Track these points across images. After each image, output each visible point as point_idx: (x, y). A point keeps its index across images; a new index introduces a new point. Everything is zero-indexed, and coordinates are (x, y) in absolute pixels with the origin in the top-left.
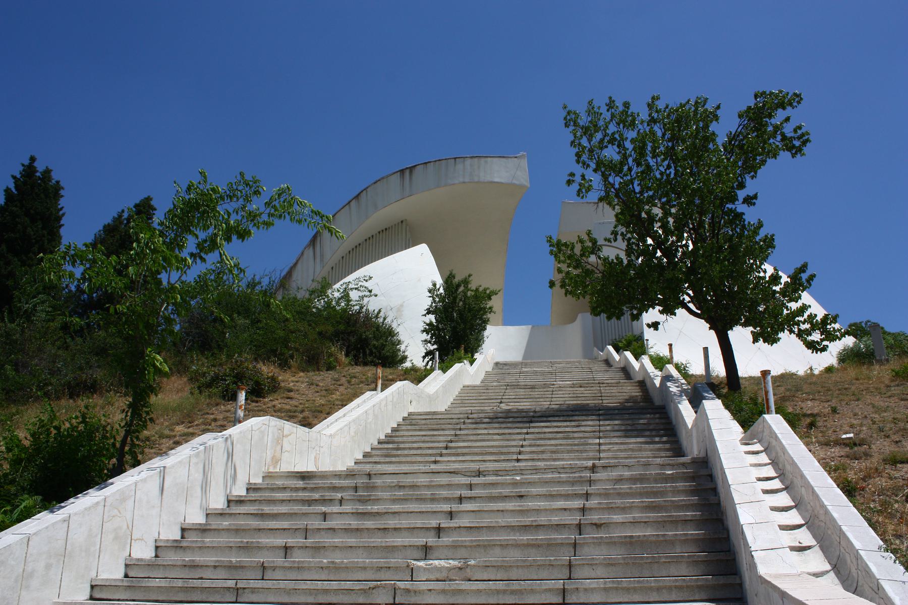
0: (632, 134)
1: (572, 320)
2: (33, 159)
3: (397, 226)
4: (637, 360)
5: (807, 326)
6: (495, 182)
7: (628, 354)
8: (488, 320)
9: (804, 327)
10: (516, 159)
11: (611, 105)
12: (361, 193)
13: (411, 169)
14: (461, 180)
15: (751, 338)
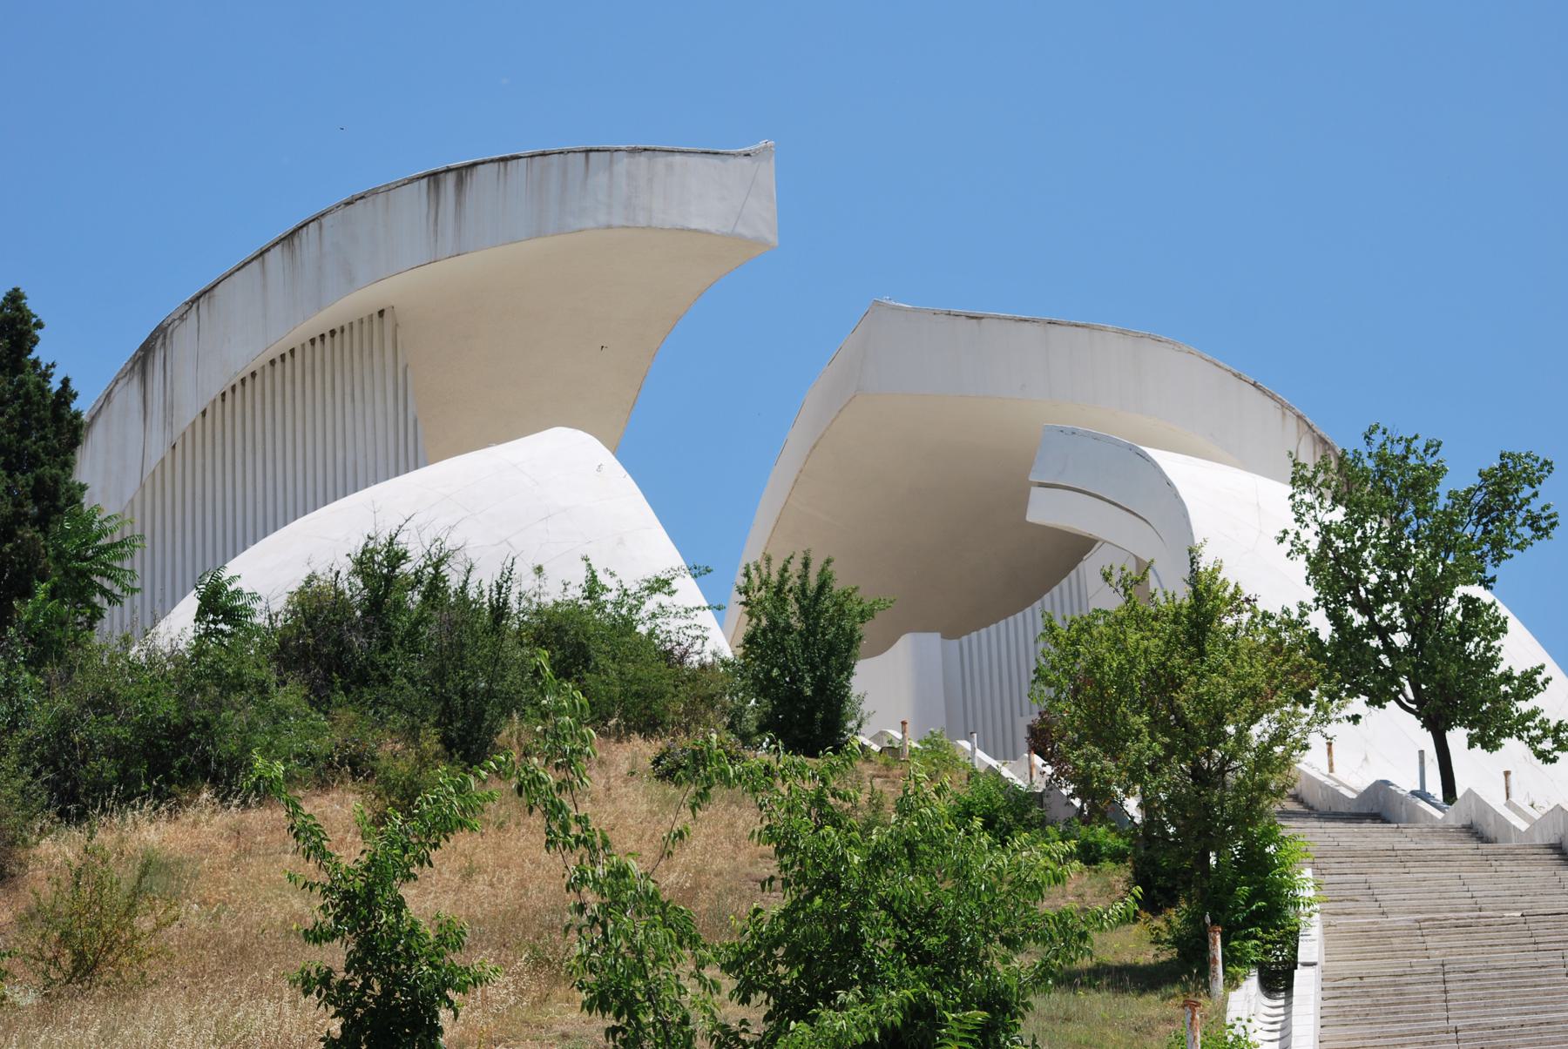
3: (366, 326)
5: (1538, 732)
6: (690, 230)
9: (1534, 733)
10: (746, 160)
12: (301, 227)
13: (463, 172)
14: (602, 219)
15: (1466, 741)
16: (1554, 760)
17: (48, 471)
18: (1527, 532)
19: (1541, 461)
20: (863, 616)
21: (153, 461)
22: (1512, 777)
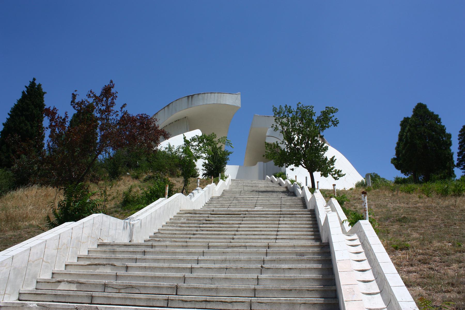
0: (291, 115)
1: (255, 164)
2: (34, 79)
4: (284, 180)
7: (281, 178)
8: (227, 163)
11: (286, 106)
13: (192, 96)
14: (213, 102)
16: (338, 179)
19: (335, 109)
22: (319, 183)
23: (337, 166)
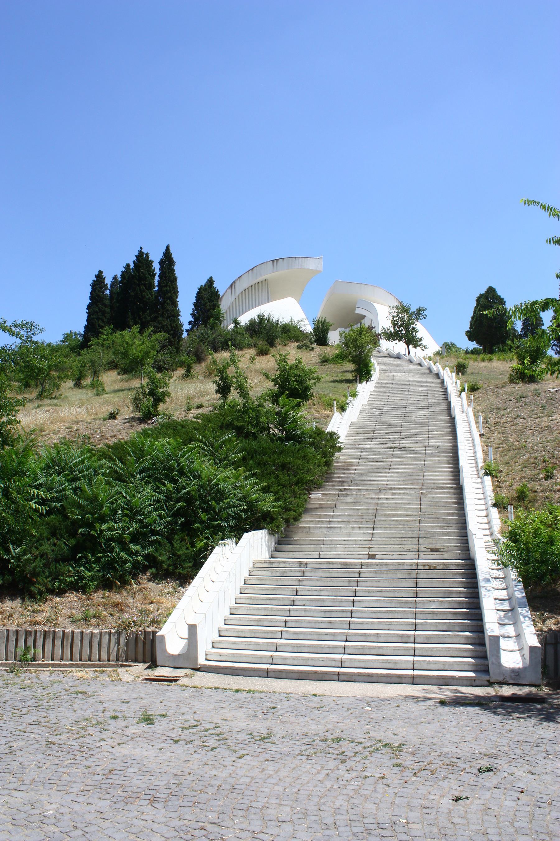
17: (215, 302)
18: (422, 318)
20: (330, 326)
21: (232, 300)
23: (424, 342)
